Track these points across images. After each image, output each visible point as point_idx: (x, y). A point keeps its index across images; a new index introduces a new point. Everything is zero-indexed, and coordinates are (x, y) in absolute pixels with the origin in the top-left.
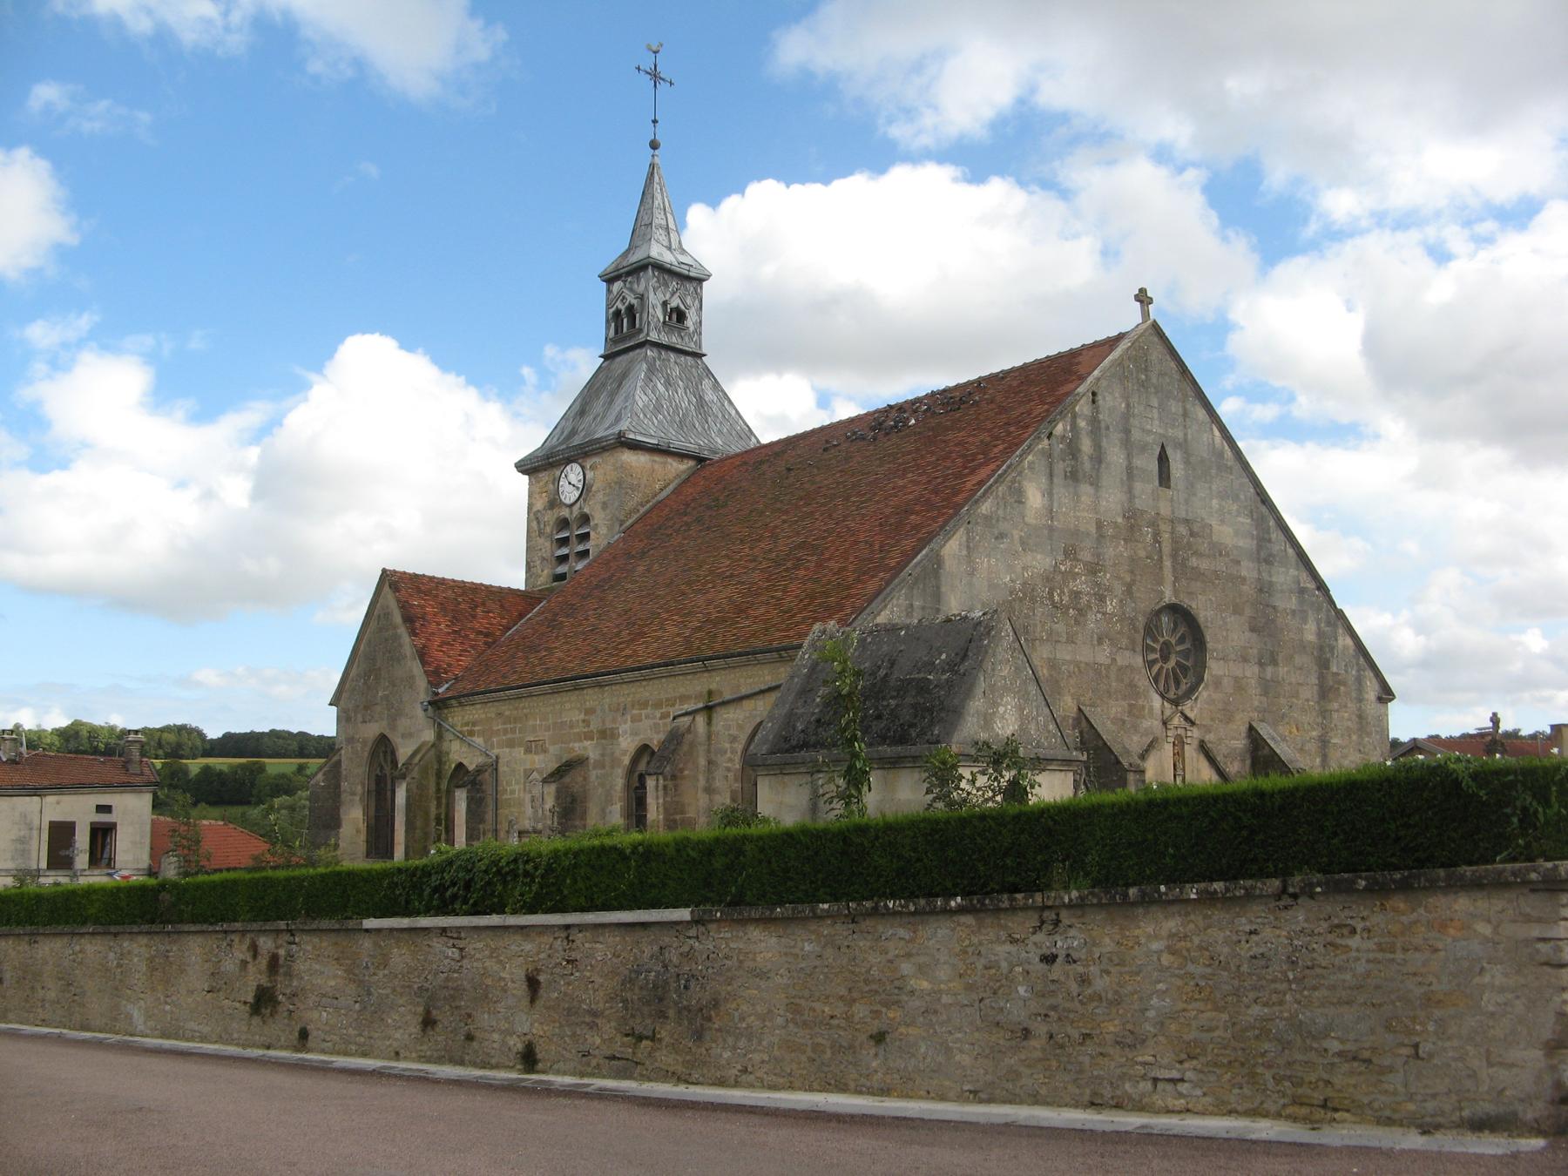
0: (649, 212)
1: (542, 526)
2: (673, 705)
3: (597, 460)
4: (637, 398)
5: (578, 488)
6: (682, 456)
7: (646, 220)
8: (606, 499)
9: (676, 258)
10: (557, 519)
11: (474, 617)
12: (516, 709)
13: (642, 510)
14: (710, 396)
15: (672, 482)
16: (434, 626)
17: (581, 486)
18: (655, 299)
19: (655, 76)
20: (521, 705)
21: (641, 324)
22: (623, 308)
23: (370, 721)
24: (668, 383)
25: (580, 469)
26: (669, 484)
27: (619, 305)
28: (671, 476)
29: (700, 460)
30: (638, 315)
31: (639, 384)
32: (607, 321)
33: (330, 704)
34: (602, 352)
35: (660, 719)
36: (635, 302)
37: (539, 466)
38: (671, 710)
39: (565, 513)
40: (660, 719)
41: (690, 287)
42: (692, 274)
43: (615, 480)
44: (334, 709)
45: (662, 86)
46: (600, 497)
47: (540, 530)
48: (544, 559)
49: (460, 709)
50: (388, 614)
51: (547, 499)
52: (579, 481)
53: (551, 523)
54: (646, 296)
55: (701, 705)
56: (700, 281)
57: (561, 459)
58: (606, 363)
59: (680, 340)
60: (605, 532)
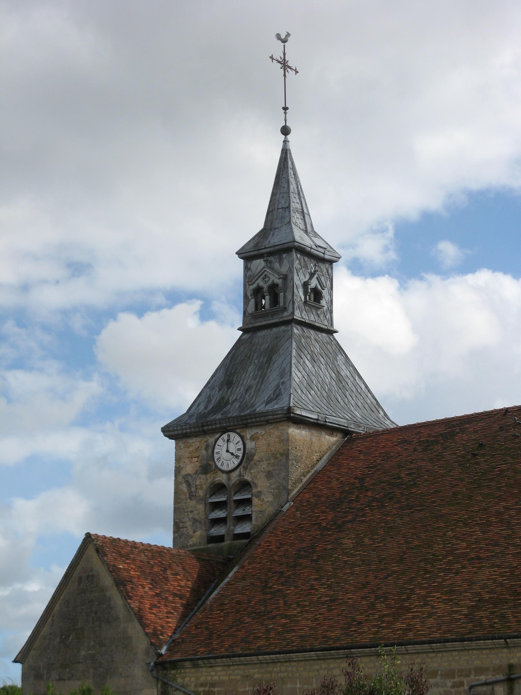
0: (286, 196)
1: (193, 489)
2: (468, 676)
3: (259, 431)
4: (293, 374)
5: (237, 457)
6: (332, 430)
7: (283, 203)
8: (271, 468)
9: (313, 242)
10: (212, 484)
11: (167, 579)
12: (270, 672)
13: (305, 480)
14: (345, 372)
15: (325, 453)
16: (140, 589)
17: (240, 454)
18: (299, 279)
19: (284, 65)
20: (275, 670)
21: (284, 303)
22: (265, 286)
23: (69, 679)
24: (313, 360)
25: (239, 439)
26: (323, 456)
27: (260, 282)
28: (325, 448)
29: (345, 432)
30: (282, 294)
31: (293, 362)
32: (245, 296)
33: (15, 661)
34: (241, 325)
35: (452, 687)
36: (279, 282)
37: (191, 432)
38: (465, 680)
39: (222, 478)
40: (452, 687)
41: (324, 267)
42: (327, 257)
43: (281, 451)
44: (19, 667)
45: (290, 74)
46: (264, 466)
47: (190, 492)
48: (195, 520)
49: (193, 670)
50: (93, 576)
51: (198, 464)
52: (239, 450)
53: (204, 487)
54: (290, 277)
55: (501, 677)
56: (331, 262)
57: (217, 428)
58: (245, 337)
59: (317, 318)
60: (270, 499)
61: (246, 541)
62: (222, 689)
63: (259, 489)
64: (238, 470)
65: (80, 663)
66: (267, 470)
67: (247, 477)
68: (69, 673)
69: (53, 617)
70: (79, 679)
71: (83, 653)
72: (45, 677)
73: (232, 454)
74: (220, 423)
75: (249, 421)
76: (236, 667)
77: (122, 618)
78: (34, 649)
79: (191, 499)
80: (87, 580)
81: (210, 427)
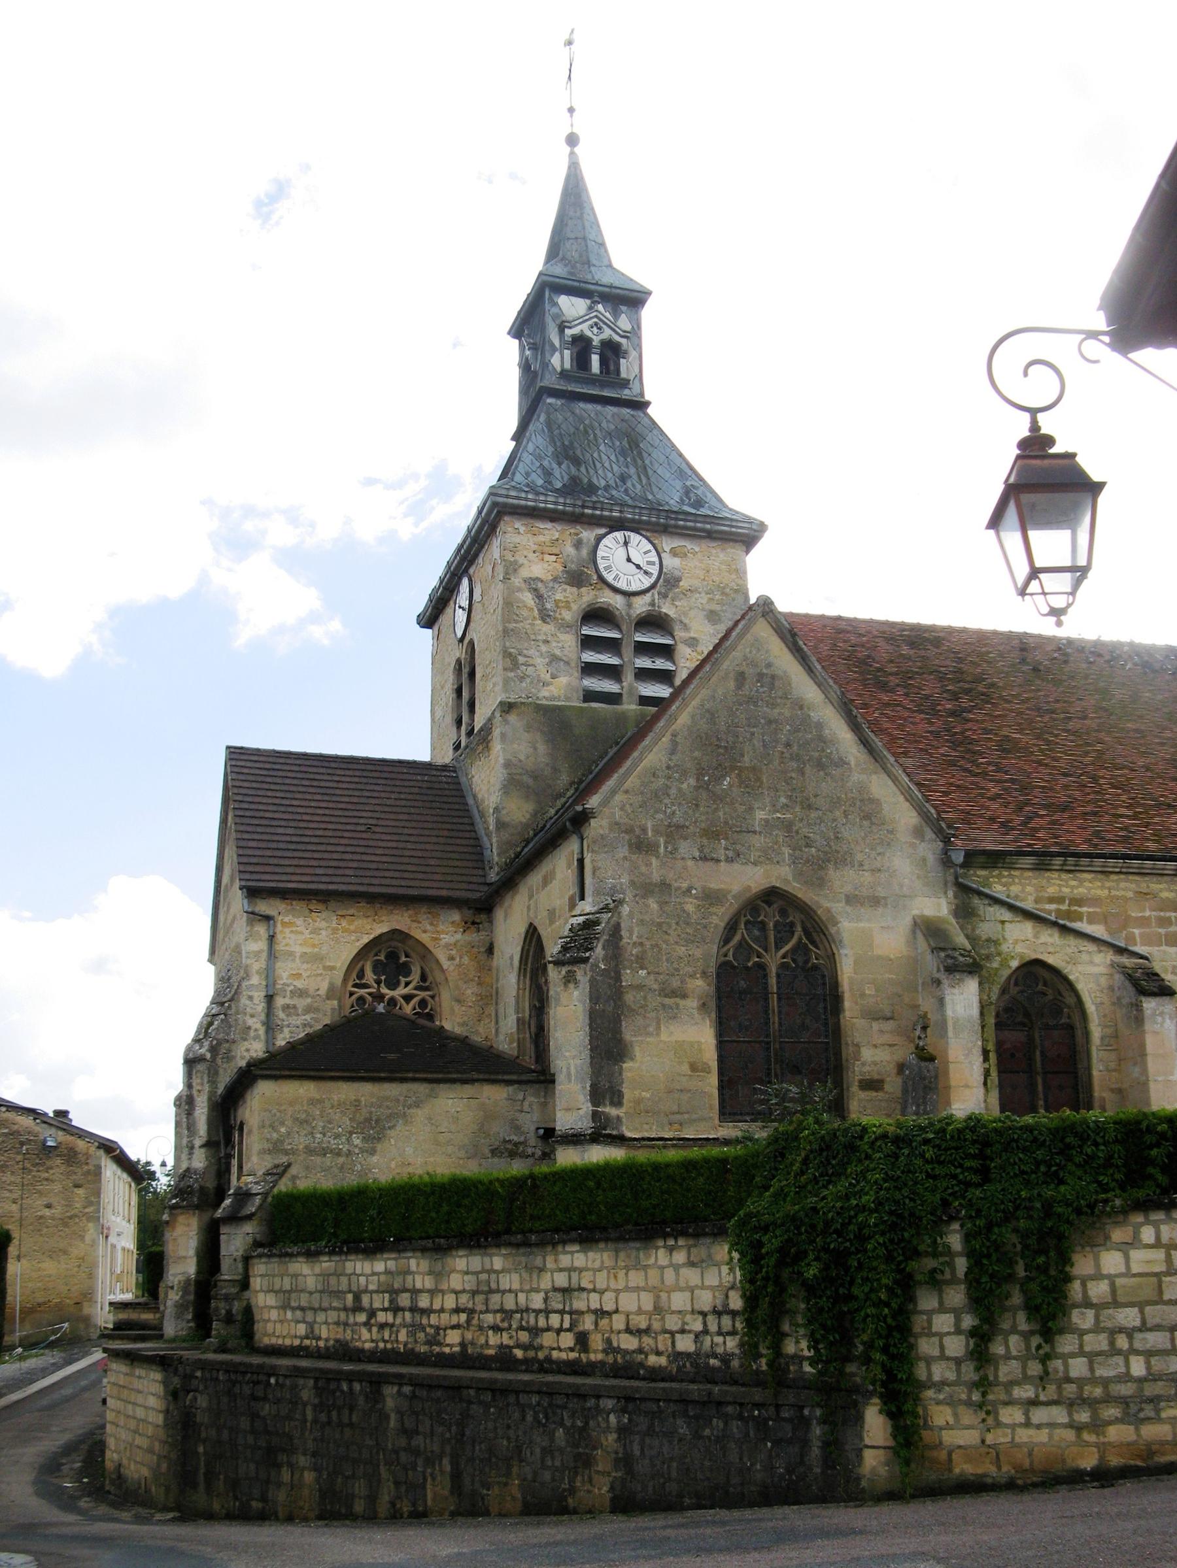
3: (689, 545)
23: (729, 860)
39: (608, 599)
48: (554, 659)
50: (773, 677)
61: (654, 709)
62: (1098, 910)
63: (692, 635)
64: (649, 595)
65: (755, 832)
66: (707, 607)
67: (667, 609)
68: (726, 849)
69: (674, 735)
70: (755, 864)
71: (760, 815)
72: (662, 850)
73: (638, 567)
74: (621, 512)
75: (673, 522)
76: (1122, 876)
77: (853, 763)
78: (627, 792)
79: (544, 621)
80: (758, 681)
81: (598, 512)
